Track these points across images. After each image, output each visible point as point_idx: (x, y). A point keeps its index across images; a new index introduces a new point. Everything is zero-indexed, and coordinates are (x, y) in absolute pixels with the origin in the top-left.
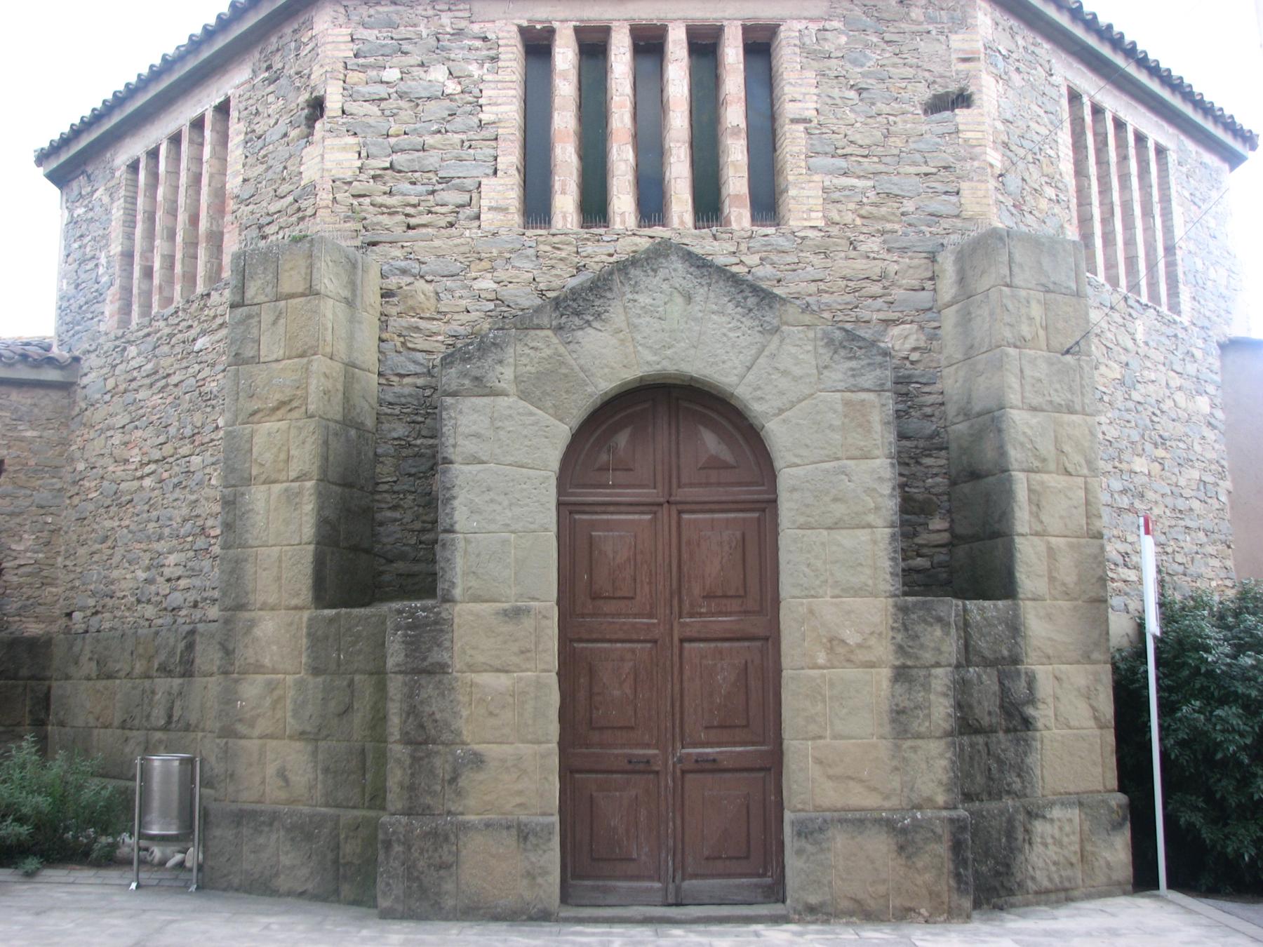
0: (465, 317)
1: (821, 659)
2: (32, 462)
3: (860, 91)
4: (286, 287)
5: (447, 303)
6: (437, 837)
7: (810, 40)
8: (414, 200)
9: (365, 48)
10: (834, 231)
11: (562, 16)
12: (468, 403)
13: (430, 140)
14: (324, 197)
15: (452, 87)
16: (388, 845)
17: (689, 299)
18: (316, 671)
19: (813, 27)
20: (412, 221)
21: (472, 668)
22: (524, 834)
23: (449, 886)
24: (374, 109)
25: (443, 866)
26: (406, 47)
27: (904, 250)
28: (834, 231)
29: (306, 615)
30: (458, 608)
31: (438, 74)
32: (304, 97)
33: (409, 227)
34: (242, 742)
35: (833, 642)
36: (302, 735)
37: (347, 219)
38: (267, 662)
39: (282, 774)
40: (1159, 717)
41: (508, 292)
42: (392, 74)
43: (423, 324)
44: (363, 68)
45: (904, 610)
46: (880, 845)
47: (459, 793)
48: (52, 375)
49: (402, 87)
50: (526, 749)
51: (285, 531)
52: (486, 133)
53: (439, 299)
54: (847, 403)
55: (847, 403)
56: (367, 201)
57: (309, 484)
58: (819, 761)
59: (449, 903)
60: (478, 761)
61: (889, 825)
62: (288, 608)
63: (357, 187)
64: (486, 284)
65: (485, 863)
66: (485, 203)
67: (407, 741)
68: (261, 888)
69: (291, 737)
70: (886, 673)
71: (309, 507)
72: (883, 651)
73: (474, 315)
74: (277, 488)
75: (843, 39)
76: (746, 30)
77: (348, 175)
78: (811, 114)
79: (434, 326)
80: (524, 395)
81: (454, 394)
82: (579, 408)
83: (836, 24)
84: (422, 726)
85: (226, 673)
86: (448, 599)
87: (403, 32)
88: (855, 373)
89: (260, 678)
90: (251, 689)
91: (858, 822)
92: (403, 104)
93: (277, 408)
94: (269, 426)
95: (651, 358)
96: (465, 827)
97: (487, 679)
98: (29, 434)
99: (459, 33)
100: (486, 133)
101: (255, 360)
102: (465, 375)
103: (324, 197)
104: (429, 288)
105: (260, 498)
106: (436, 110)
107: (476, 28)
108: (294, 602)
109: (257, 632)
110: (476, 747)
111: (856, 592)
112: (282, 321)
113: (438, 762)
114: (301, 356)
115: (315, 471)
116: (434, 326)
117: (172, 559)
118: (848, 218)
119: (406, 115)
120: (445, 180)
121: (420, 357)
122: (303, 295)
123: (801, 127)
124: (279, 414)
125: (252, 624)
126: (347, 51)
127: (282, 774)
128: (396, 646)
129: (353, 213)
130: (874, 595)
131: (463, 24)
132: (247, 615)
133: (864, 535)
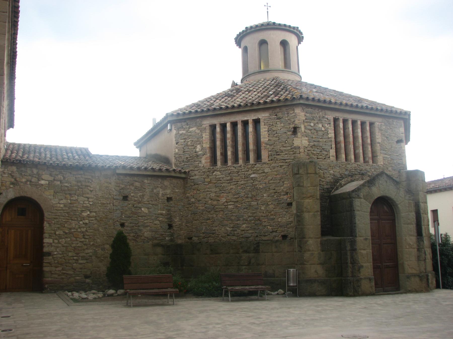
0: (329, 178)
1: (408, 247)
2: (178, 198)
3: (387, 138)
4: (309, 172)
5: (325, 175)
6: (358, 281)
7: (379, 127)
8: (318, 153)
9: (307, 118)
10: (385, 165)
11: (341, 116)
12: (357, 200)
13: (321, 140)
14: (302, 150)
15: (323, 129)
16: (350, 283)
17: (386, 182)
18: (323, 251)
19: (380, 124)
20: (319, 157)
21: (360, 249)
22: (370, 279)
23: (360, 290)
24: (309, 132)
25: (359, 286)
26: (315, 119)
27: (395, 170)
28: (385, 165)
29: (319, 240)
30: (357, 238)
31: (320, 126)
32: (292, 126)
33: (318, 158)
34: (306, 266)
35: (409, 244)
36: (320, 264)
37: (307, 155)
38: (311, 249)
39: (316, 271)
40: (440, 257)
41: (336, 174)
42: (312, 124)
43: (322, 179)
44: (307, 122)
45: (418, 239)
46: (417, 279)
47: (360, 273)
48: (183, 176)
49: (315, 127)
50: (369, 264)
51: (313, 221)
52: (330, 140)
53: (324, 174)
54: (409, 202)
55: (409, 202)
56: (310, 152)
57: (319, 213)
58: (408, 265)
59: (360, 293)
60: (362, 267)
61: (419, 276)
62: (315, 238)
63: (309, 149)
64: (332, 172)
65: (366, 285)
66: (331, 155)
67: (351, 263)
68: (313, 295)
69: (317, 264)
70: (416, 250)
71: (319, 218)
72: (415, 246)
73: (330, 178)
74: (311, 213)
75: (384, 127)
76: (370, 123)
77: (307, 146)
78: (380, 142)
79: (324, 180)
80: (365, 199)
81: (354, 198)
82: (372, 201)
83: (383, 124)
84: (354, 260)
85: (300, 252)
86: (356, 237)
87: (314, 115)
88: (410, 197)
89: (309, 252)
90: (307, 255)
91: (414, 275)
92: (315, 131)
93: (309, 197)
94: (307, 200)
95: (382, 193)
96: (361, 279)
97: (362, 251)
98: (177, 191)
99: (323, 117)
100: (330, 140)
101: (303, 186)
102: (356, 194)
103: (302, 150)
104: (322, 172)
105: (307, 216)
106: (320, 133)
107: (326, 116)
108: (317, 237)
109: (308, 243)
110: (362, 264)
111: (411, 235)
112: (309, 179)
113: (356, 267)
114: (315, 186)
115: (319, 209)
116: (324, 180)
117: (244, 226)
118: (387, 163)
119: (316, 134)
120: (323, 149)
121: (322, 186)
122: (314, 174)
123: (379, 144)
124: (310, 198)
125: (307, 241)
126: (304, 118)
127: (316, 271)
128: (349, 246)
129: (308, 155)
130: (414, 236)
131: (324, 115)
132: (306, 239)
133: (412, 226)
